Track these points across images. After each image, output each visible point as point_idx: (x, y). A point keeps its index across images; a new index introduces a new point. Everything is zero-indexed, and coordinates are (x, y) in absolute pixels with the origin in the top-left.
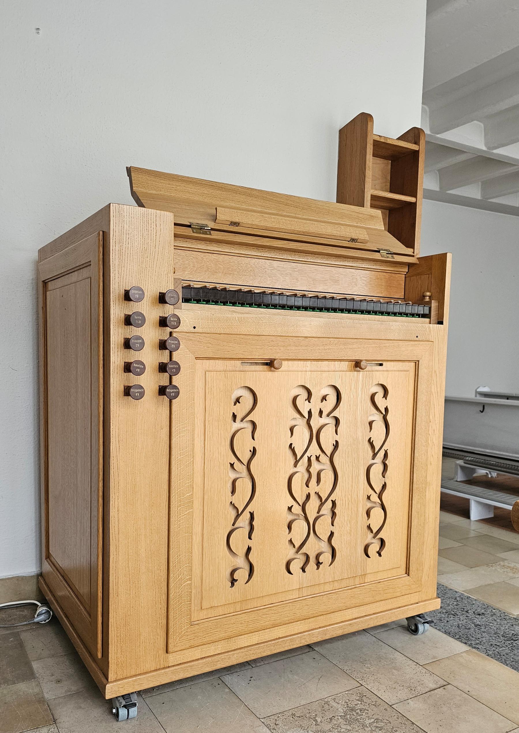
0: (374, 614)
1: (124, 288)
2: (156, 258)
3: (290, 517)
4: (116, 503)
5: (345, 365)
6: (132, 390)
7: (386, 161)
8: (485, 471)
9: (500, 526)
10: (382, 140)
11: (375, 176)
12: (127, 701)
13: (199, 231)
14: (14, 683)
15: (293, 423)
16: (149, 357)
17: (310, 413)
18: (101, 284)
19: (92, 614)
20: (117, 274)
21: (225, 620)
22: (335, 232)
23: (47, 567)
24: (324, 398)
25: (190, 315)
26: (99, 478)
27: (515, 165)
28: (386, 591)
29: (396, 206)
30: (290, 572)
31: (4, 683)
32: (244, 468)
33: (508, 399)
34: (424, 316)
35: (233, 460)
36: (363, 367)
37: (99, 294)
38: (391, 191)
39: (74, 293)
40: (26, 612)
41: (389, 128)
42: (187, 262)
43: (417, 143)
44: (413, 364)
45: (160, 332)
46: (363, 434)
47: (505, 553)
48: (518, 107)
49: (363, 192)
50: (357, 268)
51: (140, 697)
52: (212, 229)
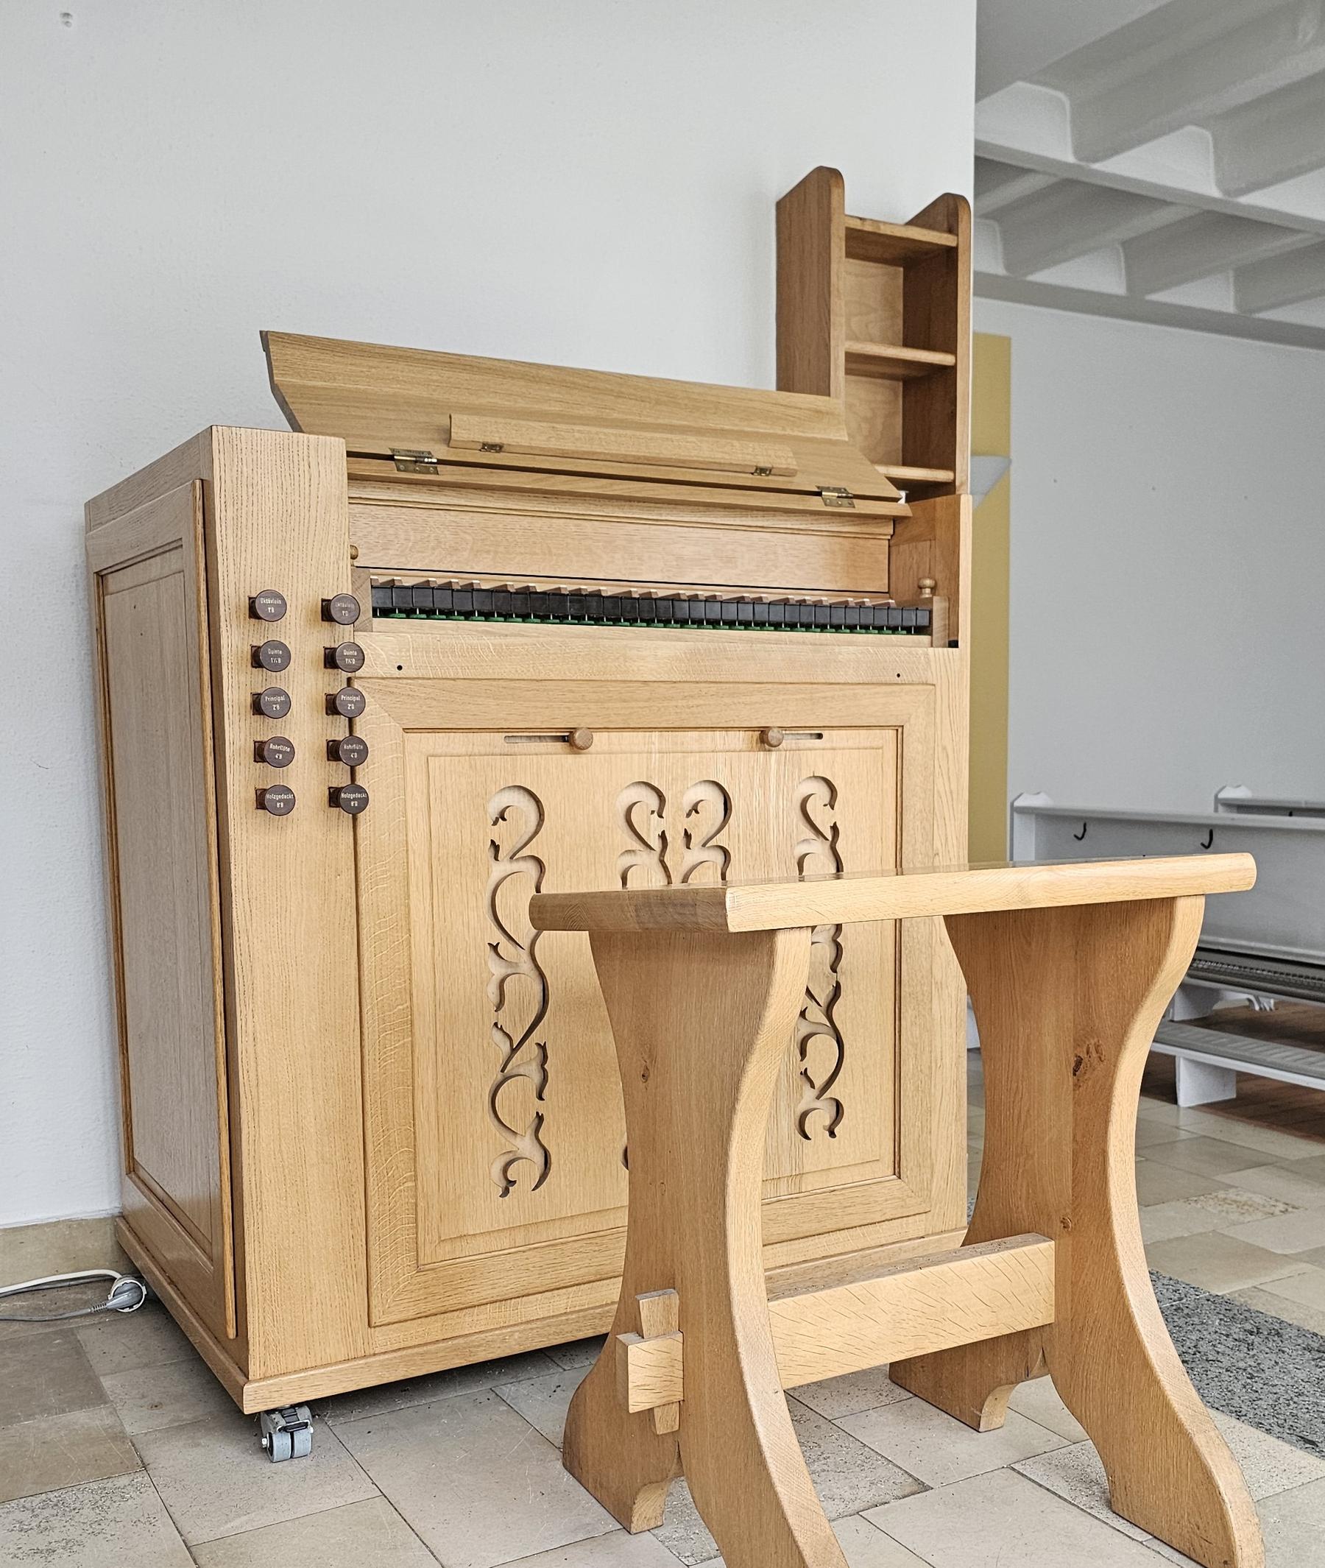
0: (824, 1258)
1: (248, 594)
2: (312, 532)
4: (250, 1024)
5: (739, 740)
6: (268, 796)
7: (891, 269)
8: (1245, 996)
9: (1284, 1126)
10: (868, 228)
11: (860, 310)
13: (411, 467)
14: (64, 1411)
15: (627, 860)
16: (305, 729)
18: (203, 587)
20: (231, 566)
21: (489, 1262)
22: (719, 455)
23: (138, 1199)
25: (387, 644)
26: (214, 976)
27: (1299, 231)
28: (850, 1210)
29: (914, 373)
31: (42, 1413)
32: (525, 956)
33: (1291, 815)
34: (920, 630)
35: (498, 937)
36: (773, 742)
37: (199, 606)
39: (153, 599)
40: (89, 1294)
41: (887, 195)
42: (391, 531)
43: (952, 230)
44: (893, 733)
45: (326, 679)
47: (1237, 1174)
48: (1323, 78)
49: (828, 346)
50: (775, 530)
51: (322, 1425)
52: (440, 462)
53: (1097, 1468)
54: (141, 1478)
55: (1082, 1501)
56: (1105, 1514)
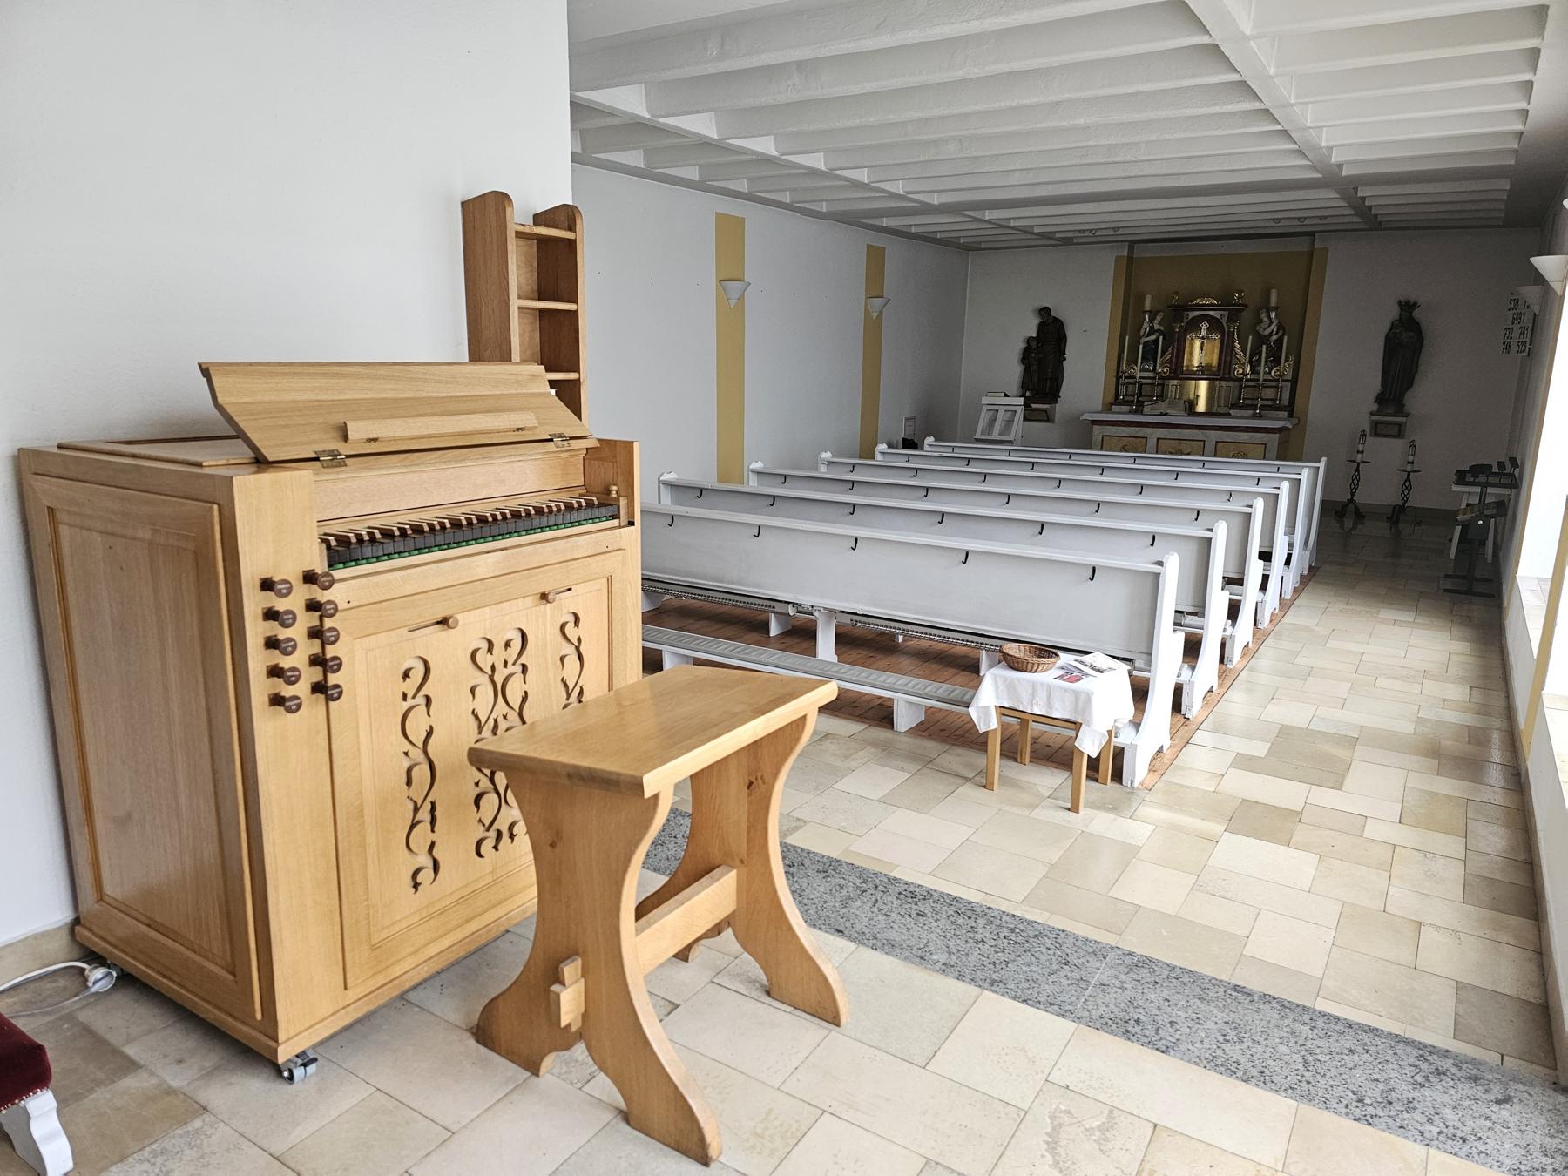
3: (478, 791)
5: (529, 601)
12: (306, 1060)
17: (493, 668)
19: (237, 968)
24: (507, 645)
30: (479, 855)
35: (407, 747)
38: (540, 299)
43: (571, 228)
46: (554, 675)
52: (348, 456)
53: (757, 972)
54: (208, 1118)
55: (755, 994)
56: (768, 1000)
